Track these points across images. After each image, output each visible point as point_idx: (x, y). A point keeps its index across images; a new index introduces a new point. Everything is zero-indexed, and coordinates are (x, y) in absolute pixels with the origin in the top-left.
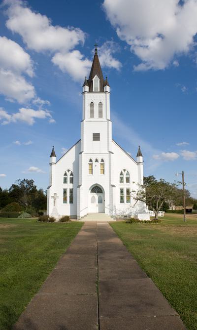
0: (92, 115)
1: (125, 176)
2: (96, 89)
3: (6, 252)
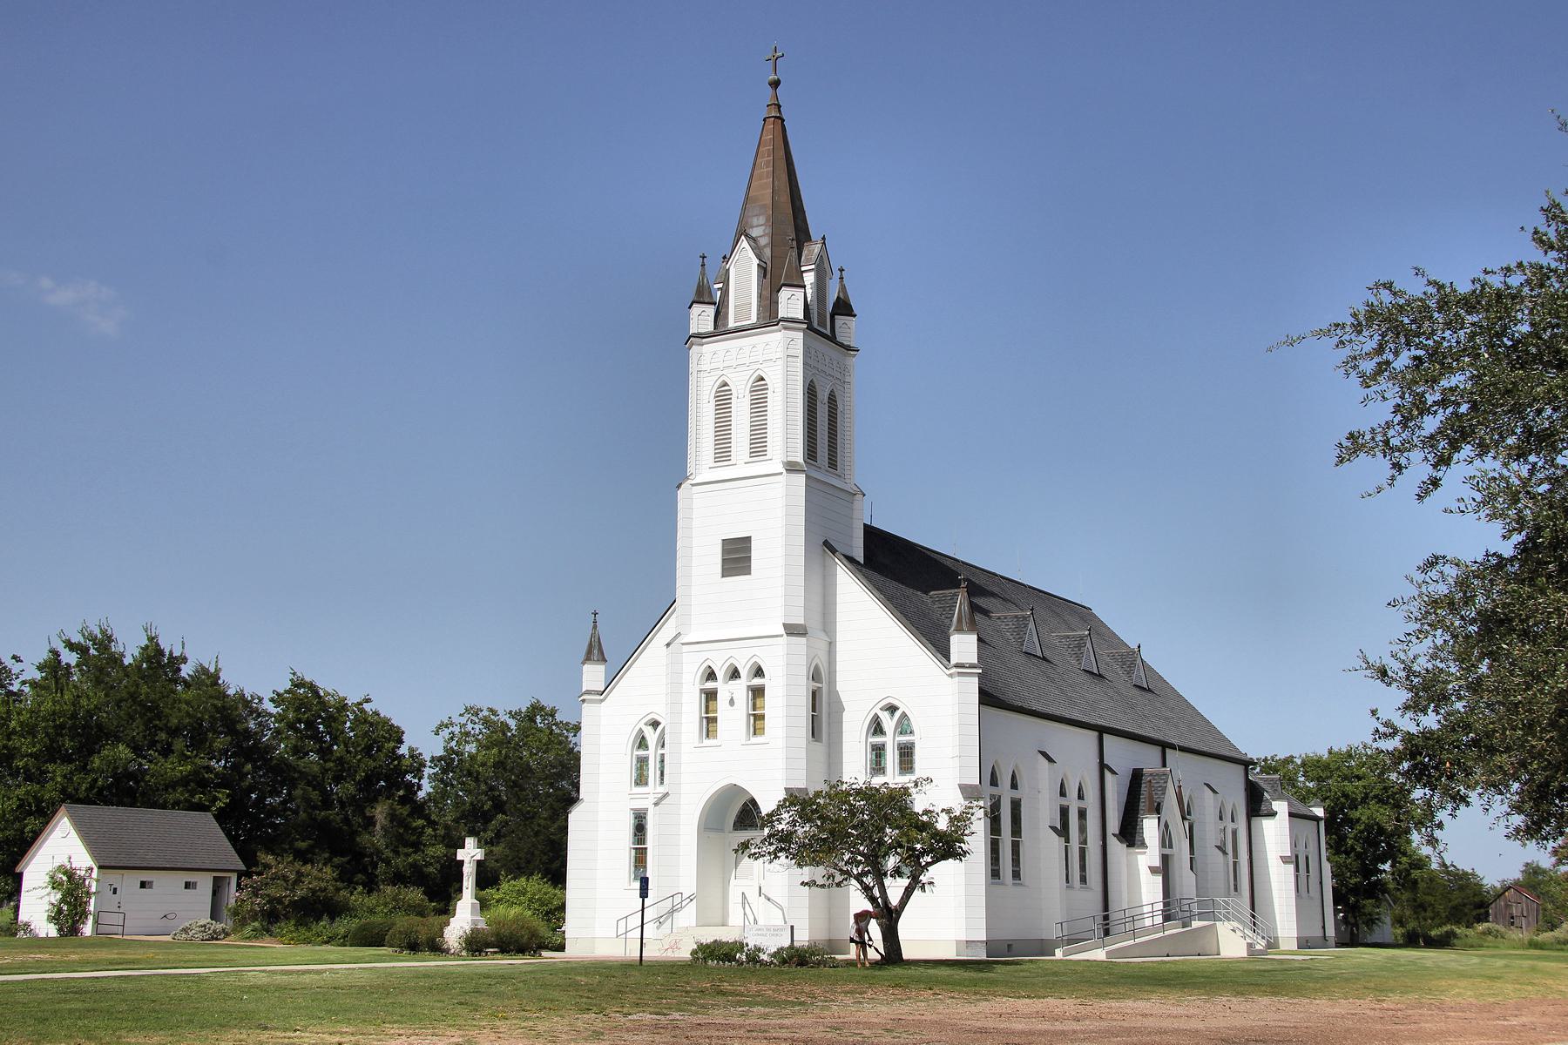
0: (723, 453)
1: (890, 741)
2: (743, 309)
3: (146, 725)
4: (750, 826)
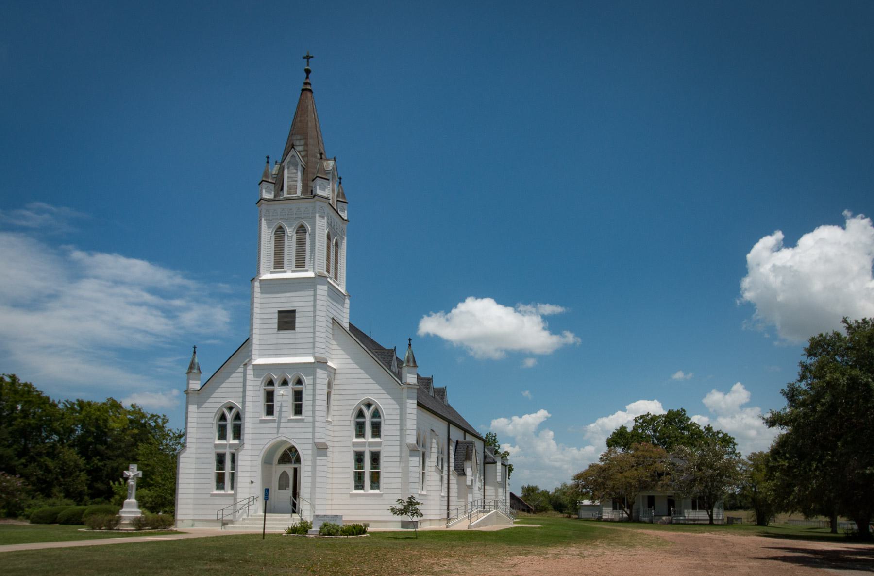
4: (287, 462)
